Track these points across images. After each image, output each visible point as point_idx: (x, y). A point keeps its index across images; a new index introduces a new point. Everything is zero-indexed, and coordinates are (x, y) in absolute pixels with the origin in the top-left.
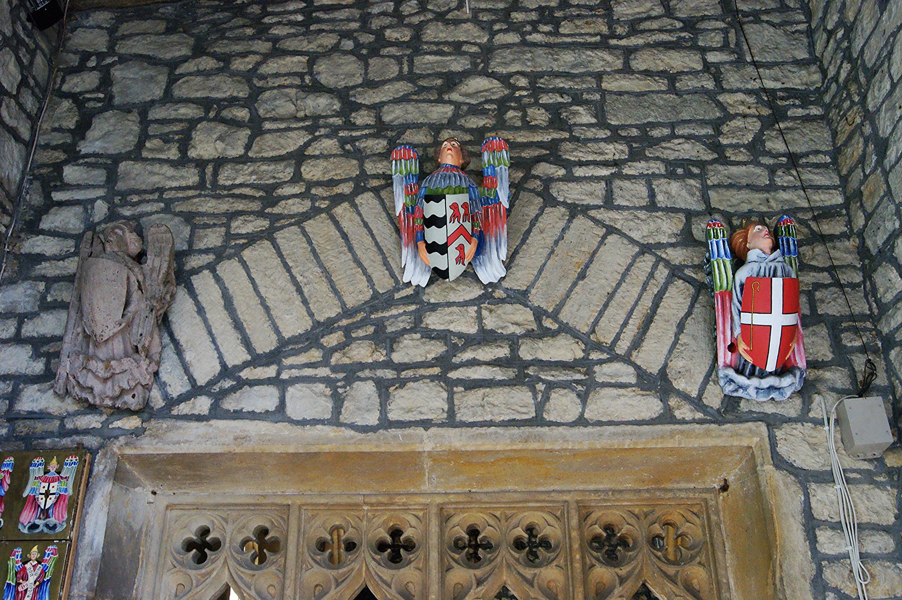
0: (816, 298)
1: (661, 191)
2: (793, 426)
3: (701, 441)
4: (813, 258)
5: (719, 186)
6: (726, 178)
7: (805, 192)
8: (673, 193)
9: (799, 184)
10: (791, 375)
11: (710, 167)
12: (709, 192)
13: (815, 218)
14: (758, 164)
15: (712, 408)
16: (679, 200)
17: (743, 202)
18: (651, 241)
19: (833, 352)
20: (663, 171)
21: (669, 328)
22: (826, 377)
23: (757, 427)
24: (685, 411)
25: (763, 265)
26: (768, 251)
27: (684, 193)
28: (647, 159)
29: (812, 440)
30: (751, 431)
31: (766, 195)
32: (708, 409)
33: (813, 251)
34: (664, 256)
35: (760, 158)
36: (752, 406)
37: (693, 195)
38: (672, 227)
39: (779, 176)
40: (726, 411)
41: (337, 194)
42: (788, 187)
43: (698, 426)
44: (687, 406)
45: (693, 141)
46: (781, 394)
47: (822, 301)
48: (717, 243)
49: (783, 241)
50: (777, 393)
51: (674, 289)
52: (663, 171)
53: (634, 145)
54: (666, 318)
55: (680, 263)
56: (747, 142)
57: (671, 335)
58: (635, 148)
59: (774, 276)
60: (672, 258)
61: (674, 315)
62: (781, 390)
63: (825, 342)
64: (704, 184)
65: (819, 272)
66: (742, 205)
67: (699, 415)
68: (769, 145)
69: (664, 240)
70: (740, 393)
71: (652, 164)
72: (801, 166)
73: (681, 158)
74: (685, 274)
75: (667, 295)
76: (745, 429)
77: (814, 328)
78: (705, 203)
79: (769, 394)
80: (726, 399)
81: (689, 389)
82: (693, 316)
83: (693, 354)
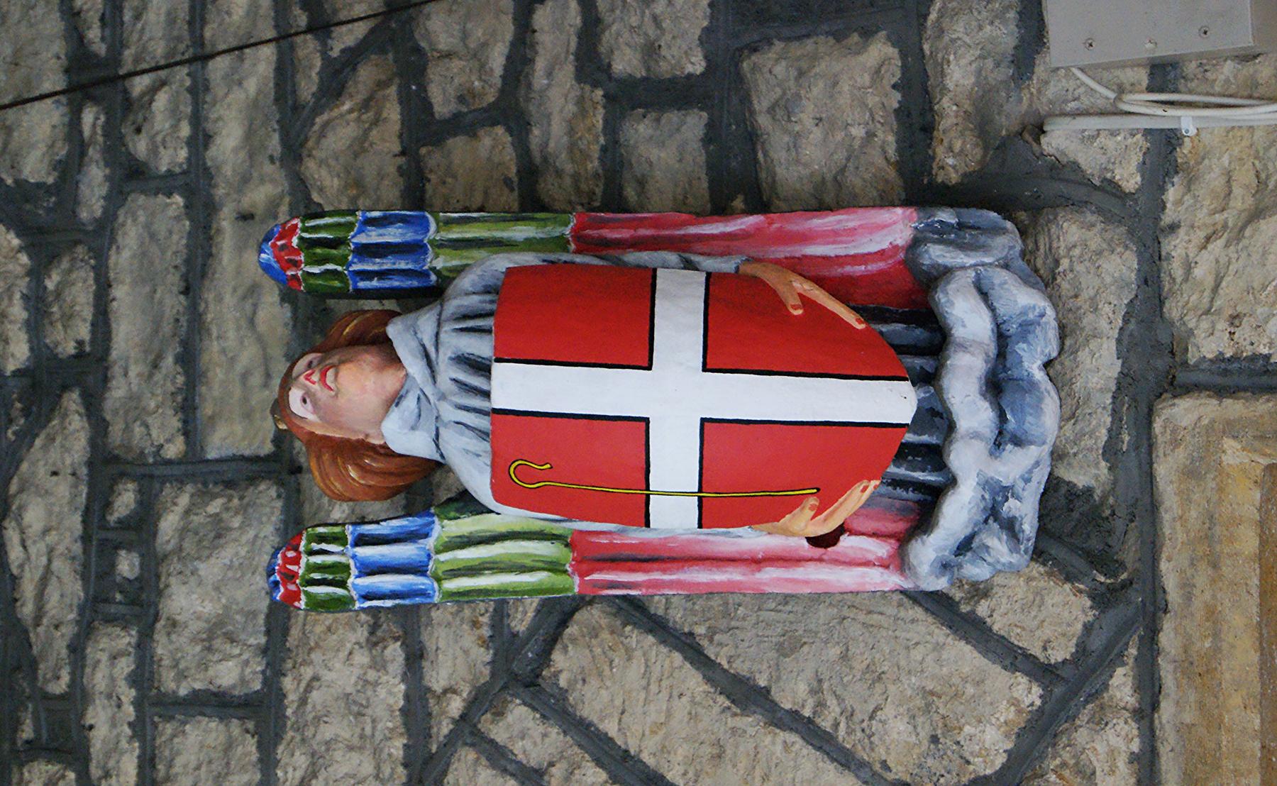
0: (640, 73)
1: (204, 666)
2: (1178, 273)
3: (1236, 700)
4: (478, 56)
5: (187, 407)
6: (158, 377)
7: (212, 56)
8: (209, 608)
9: (181, 75)
10: (941, 297)
11: (116, 434)
12: (212, 454)
13: (321, 27)
14: (104, 230)
15: (1088, 628)
16: (240, 595)
17: (252, 322)
18: (397, 748)
19: (868, 34)
20: (125, 639)
21: (747, 746)
22: (969, 81)
23: (1175, 443)
24: (1101, 747)
25: (449, 413)
26: (390, 381)
27: (210, 569)
28: (79, 696)
29: (1241, 201)
30: (1191, 473)
31: (226, 222)
32: (1097, 643)
33: (449, 55)
34: (456, 706)
35: (84, 215)
36: (1087, 442)
37: (219, 532)
38: (342, 642)
39: (154, 151)
40: (1103, 560)
41: (755, 278)
42: (197, 120)
43: (1167, 711)
44: (1082, 736)
45: (13, 488)
46: (1027, 328)
47: (651, 51)
48: (370, 569)
49: (367, 275)
50: (1021, 348)
51: (588, 691)
52: (125, 639)
53: (27, 732)
54: (707, 750)
55: (485, 643)
56: (24, 258)
57: (779, 743)
58: (37, 730)
59: (486, 395)
60: (462, 671)
61: (693, 717)
62: (1013, 328)
63: (821, 67)
64: (177, 471)
65: (533, 46)
66: (262, 328)
67: (1122, 687)
68: (35, 168)
69: (392, 691)
70: (1025, 509)
71: (98, 680)
72: (115, 55)
73: (77, 548)
74: (533, 630)
75: (610, 727)
76: (1186, 500)
77: (761, 104)
78: (253, 480)
79: (1030, 386)
80: (1055, 550)
81: (1006, 714)
82: (700, 630)
83: (859, 666)
